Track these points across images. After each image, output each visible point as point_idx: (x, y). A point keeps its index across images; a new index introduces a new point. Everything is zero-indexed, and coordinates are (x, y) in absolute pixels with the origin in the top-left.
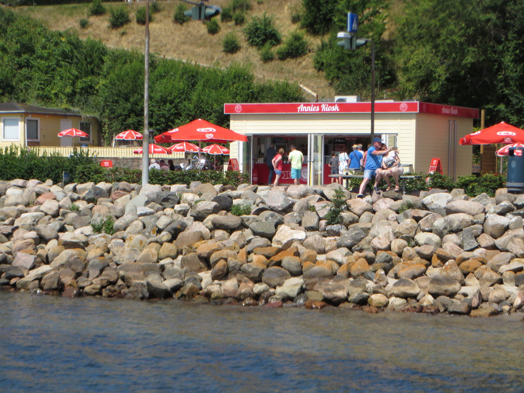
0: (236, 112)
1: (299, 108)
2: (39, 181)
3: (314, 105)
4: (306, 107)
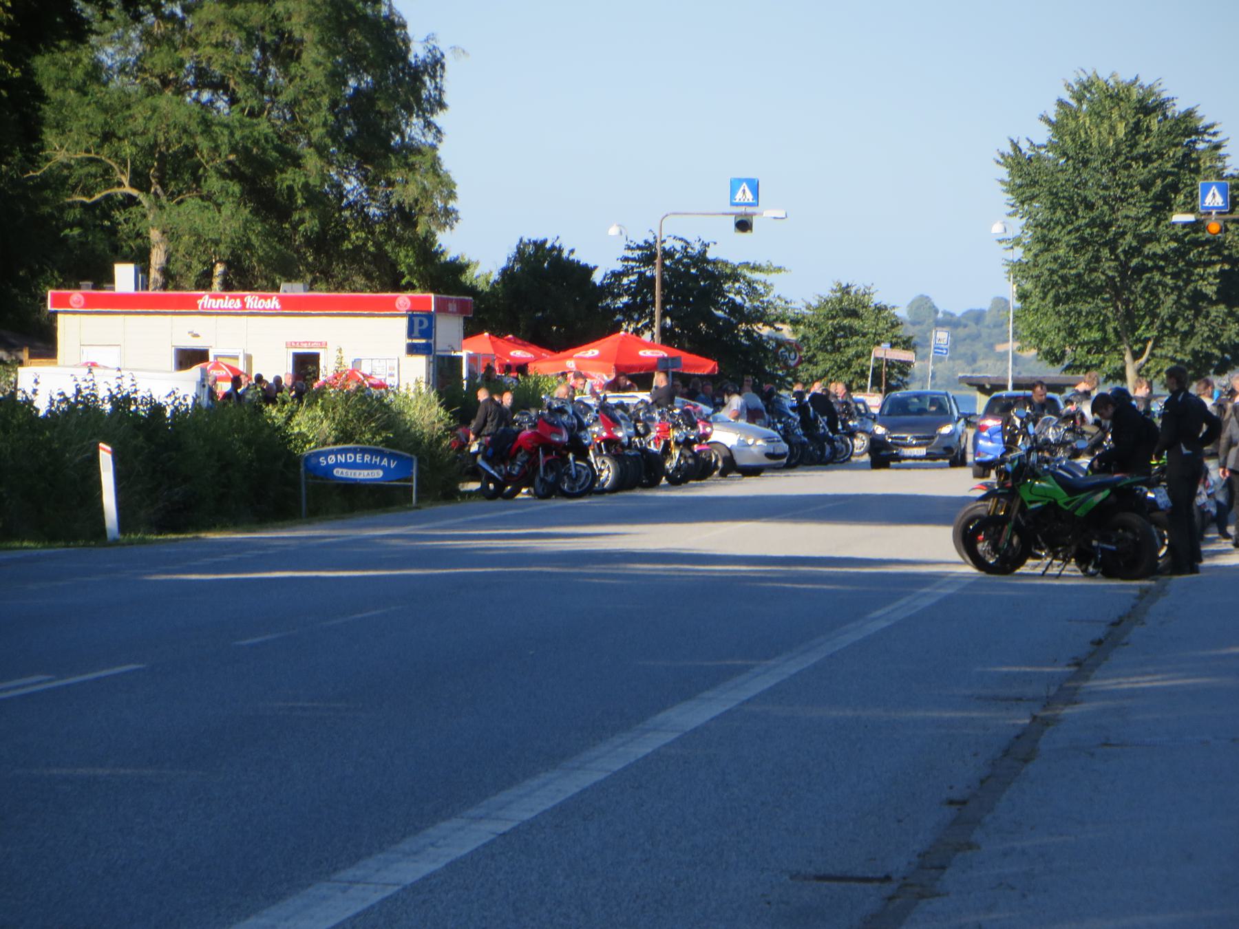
1: (200, 302)
3: (231, 297)
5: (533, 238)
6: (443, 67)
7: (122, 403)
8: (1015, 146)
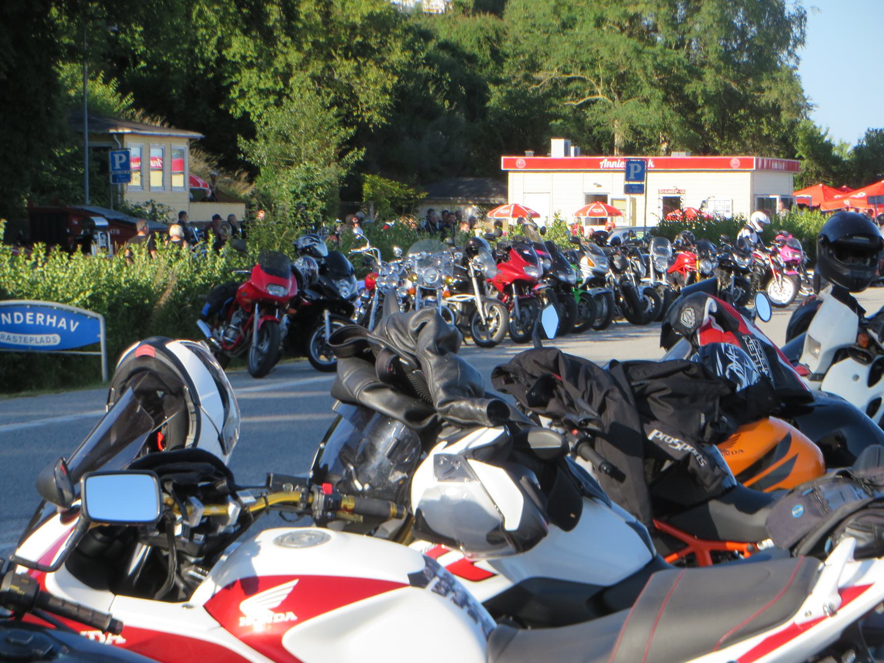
1: (601, 163)
5: (875, 128)
6: (806, 20)
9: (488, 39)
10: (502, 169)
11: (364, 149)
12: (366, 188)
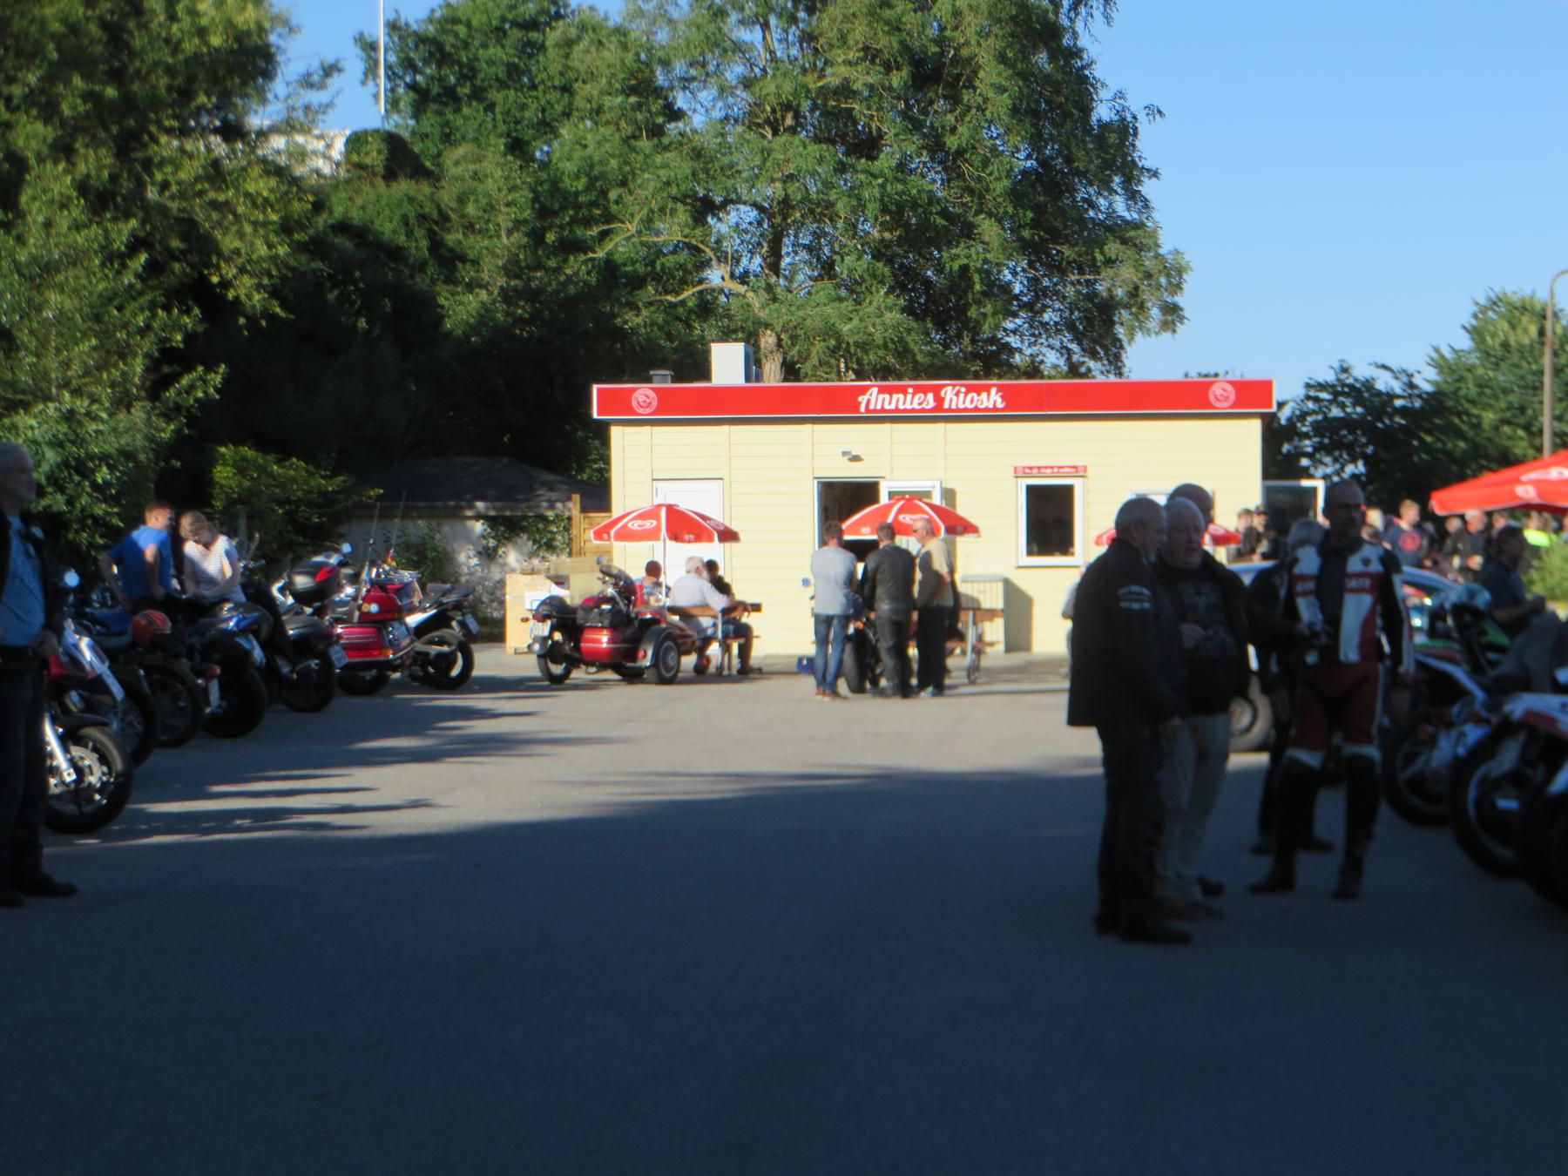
0: (1213, 407)
1: (863, 399)
2: (1494, 533)
3: (917, 390)
4: (887, 396)
7: (1076, 53)
8: (1437, 350)
9: (423, 217)
10: (595, 416)
11: (222, 368)
12: (223, 474)
